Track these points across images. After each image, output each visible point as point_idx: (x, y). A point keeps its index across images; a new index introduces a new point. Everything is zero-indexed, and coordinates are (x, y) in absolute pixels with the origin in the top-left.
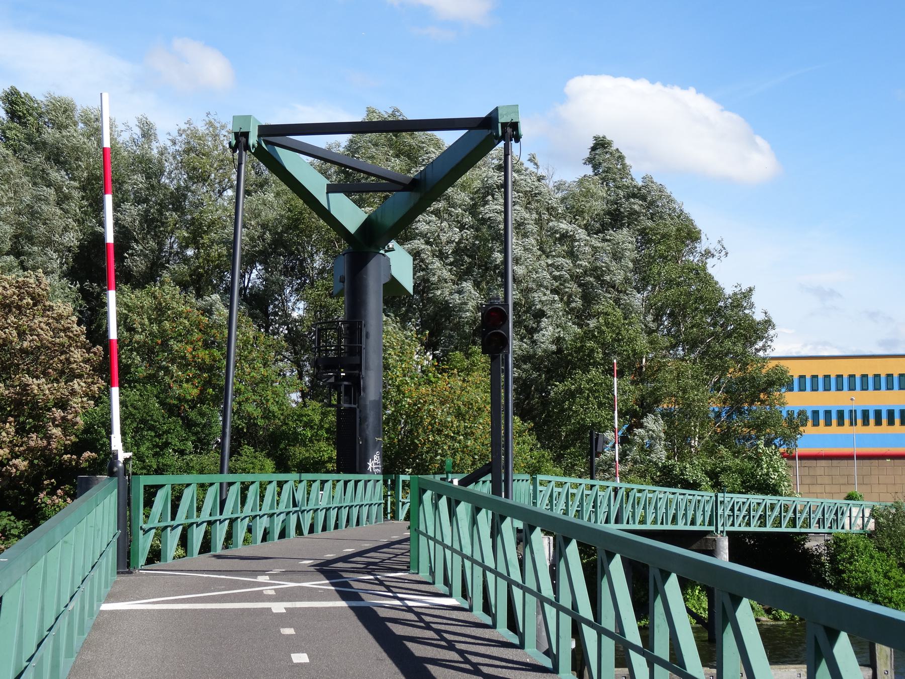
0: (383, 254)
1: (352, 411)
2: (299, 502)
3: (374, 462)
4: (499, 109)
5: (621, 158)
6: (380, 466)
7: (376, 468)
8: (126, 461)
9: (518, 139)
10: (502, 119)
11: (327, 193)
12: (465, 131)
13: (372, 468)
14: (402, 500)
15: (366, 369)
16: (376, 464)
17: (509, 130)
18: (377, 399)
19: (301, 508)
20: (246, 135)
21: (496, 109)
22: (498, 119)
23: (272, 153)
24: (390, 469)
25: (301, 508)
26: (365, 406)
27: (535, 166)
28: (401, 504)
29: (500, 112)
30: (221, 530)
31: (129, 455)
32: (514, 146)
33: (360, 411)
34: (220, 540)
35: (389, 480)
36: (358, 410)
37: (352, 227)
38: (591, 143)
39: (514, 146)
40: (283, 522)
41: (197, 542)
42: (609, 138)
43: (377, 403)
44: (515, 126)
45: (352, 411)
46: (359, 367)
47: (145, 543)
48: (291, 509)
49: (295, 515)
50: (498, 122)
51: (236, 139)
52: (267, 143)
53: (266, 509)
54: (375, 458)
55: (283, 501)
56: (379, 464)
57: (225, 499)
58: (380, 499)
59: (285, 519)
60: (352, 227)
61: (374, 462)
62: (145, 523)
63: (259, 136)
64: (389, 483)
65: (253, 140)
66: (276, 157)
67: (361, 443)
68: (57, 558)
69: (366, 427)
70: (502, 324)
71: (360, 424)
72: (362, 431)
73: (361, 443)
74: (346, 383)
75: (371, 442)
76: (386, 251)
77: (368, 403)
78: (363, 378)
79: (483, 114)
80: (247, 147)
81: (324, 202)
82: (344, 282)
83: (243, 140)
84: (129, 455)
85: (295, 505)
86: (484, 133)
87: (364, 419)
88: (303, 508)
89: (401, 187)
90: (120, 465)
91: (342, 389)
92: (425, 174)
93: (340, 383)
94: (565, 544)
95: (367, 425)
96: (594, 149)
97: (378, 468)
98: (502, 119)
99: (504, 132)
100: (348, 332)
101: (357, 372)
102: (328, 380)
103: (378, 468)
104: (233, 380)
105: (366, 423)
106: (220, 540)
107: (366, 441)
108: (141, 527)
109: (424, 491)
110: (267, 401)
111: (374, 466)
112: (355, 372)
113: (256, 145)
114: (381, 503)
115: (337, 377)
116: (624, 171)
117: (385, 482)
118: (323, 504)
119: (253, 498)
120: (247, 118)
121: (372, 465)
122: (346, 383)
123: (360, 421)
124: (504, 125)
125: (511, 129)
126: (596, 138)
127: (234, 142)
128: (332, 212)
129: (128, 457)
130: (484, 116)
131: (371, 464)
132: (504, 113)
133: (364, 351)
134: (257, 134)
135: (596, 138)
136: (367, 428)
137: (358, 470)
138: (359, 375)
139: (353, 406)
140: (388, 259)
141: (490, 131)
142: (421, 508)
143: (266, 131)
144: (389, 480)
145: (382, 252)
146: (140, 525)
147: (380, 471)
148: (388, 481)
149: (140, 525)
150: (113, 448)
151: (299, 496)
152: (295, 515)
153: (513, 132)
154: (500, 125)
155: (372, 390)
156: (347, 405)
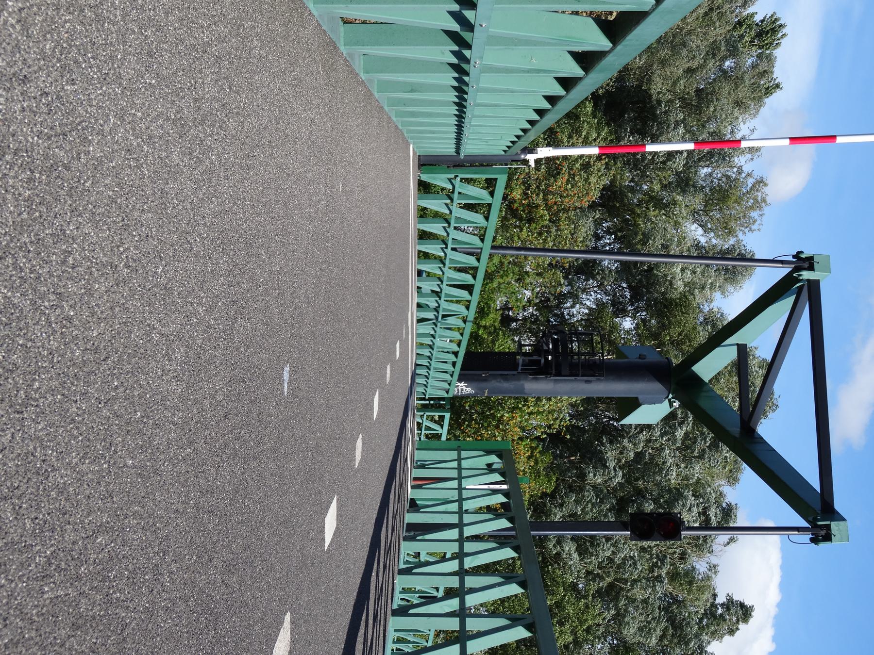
0: (667, 397)
1: (515, 366)
2: (445, 320)
3: (463, 388)
4: (844, 522)
5: (732, 632)
6: (460, 394)
7: (458, 390)
8: (526, 162)
9: (815, 541)
10: (835, 526)
11: (737, 344)
12: (818, 489)
13: (458, 386)
14: (425, 415)
15: (555, 380)
16: (462, 390)
17: (823, 532)
18: (526, 391)
19: (440, 322)
20: (811, 268)
21: (844, 519)
22: (834, 521)
23: (790, 291)
24: (455, 405)
25: (440, 322)
26: (519, 380)
27: (725, 543)
28: (422, 414)
29: (841, 523)
30: (436, 249)
31: (532, 164)
32: (807, 537)
33: (514, 375)
34: (426, 248)
35: (444, 403)
36: (515, 372)
37: (699, 368)
38: (747, 603)
39: (807, 537)
40: (427, 305)
41: (431, 228)
42: (751, 620)
43: (522, 391)
44: (828, 538)
45: (515, 366)
46: (559, 374)
47: (439, 180)
48: (441, 313)
49: (433, 317)
50: (830, 522)
51: (806, 258)
52: (800, 289)
53: (447, 290)
54: (467, 389)
55: (449, 305)
56: (462, 393)
57: (457, 251)
58: (430, 394)
59: (429, 307)
60: (699, 368)
61: (463, 388)
62: (462, 179)
63: (808, 280)
64: (442, 402)
65: (806, 275)
66: (782, 297)
67: (483, 375)
68: (524, 115)
69: (499, 380)
70: (660, 534)
71: (501, 375)
72: (495, 377)
73: (483, 375)
74: (543, 361)
75: (483, 385)
76: (669, 400)
77: (522, 382)
78: (547, 377)
79: (838, 506)
80: (797, 269)
81: (729, 341)
82: (640, 358)
83: (806, 265)
84: (532, 164)
85: (444, 316)
86: (817, 505)
87: (506, 378)
88: (439, 325)
89: (746, 418)
90: (523, 156)
91: (535, 358)
92: (761, 443)
93: (543, 356)
94: (527, 625)
95: (500, 382)
96: (742, 605)
97: (458, 392)
98: (835, 526)
99: (821, 527)
100: (591, 362)
101: (554, 372)
102: (545, 344)
103: (458, 392)
104: (558, 256)
105: (502, 381)
106: (426, 248)
107: (485, 380)
108: (457, 176)
109: (500, 456)
110: (502, 277)
111: (460, 388)
112: (554, 370)
113: (801, 278)
114: (425, 395)
115: (548, 352)
116: (716, 635)
117: (443, 399)
118: (438, 342)
119: (460, 278)
120: (827, 269)
121: (461, 386)
122: (543, 361)
123: (505, 375)
124: (828, 527)
125: (824, 534)
126: (752, 607)
127: (803, 256)
128: (717, 349)
129: (530, 164)
130: (836, 507)
131: (462, 384)
132: (841, 527)
133: (573, 378)
134: (811, 278)
135: (752, 607)
136: (497, 382)
137: (464, 372)
138: (551, 374)
139: (520, 368)
140: (661, 402)
141: (819, 512)
142: (482, 453)
143: (814, 288)
144: (444, 403)
145: (671, 396)
146: (459, 175)
147: (455, 393)
148: (444, 401)
149: (459, 175)
150: (539, 149)
151: (451, 320)
152: (433, 317)
153: (821, 536)
154: (828, 523)
155: (533, 386)
156: (521, 362)
